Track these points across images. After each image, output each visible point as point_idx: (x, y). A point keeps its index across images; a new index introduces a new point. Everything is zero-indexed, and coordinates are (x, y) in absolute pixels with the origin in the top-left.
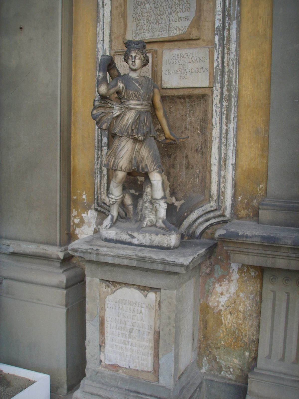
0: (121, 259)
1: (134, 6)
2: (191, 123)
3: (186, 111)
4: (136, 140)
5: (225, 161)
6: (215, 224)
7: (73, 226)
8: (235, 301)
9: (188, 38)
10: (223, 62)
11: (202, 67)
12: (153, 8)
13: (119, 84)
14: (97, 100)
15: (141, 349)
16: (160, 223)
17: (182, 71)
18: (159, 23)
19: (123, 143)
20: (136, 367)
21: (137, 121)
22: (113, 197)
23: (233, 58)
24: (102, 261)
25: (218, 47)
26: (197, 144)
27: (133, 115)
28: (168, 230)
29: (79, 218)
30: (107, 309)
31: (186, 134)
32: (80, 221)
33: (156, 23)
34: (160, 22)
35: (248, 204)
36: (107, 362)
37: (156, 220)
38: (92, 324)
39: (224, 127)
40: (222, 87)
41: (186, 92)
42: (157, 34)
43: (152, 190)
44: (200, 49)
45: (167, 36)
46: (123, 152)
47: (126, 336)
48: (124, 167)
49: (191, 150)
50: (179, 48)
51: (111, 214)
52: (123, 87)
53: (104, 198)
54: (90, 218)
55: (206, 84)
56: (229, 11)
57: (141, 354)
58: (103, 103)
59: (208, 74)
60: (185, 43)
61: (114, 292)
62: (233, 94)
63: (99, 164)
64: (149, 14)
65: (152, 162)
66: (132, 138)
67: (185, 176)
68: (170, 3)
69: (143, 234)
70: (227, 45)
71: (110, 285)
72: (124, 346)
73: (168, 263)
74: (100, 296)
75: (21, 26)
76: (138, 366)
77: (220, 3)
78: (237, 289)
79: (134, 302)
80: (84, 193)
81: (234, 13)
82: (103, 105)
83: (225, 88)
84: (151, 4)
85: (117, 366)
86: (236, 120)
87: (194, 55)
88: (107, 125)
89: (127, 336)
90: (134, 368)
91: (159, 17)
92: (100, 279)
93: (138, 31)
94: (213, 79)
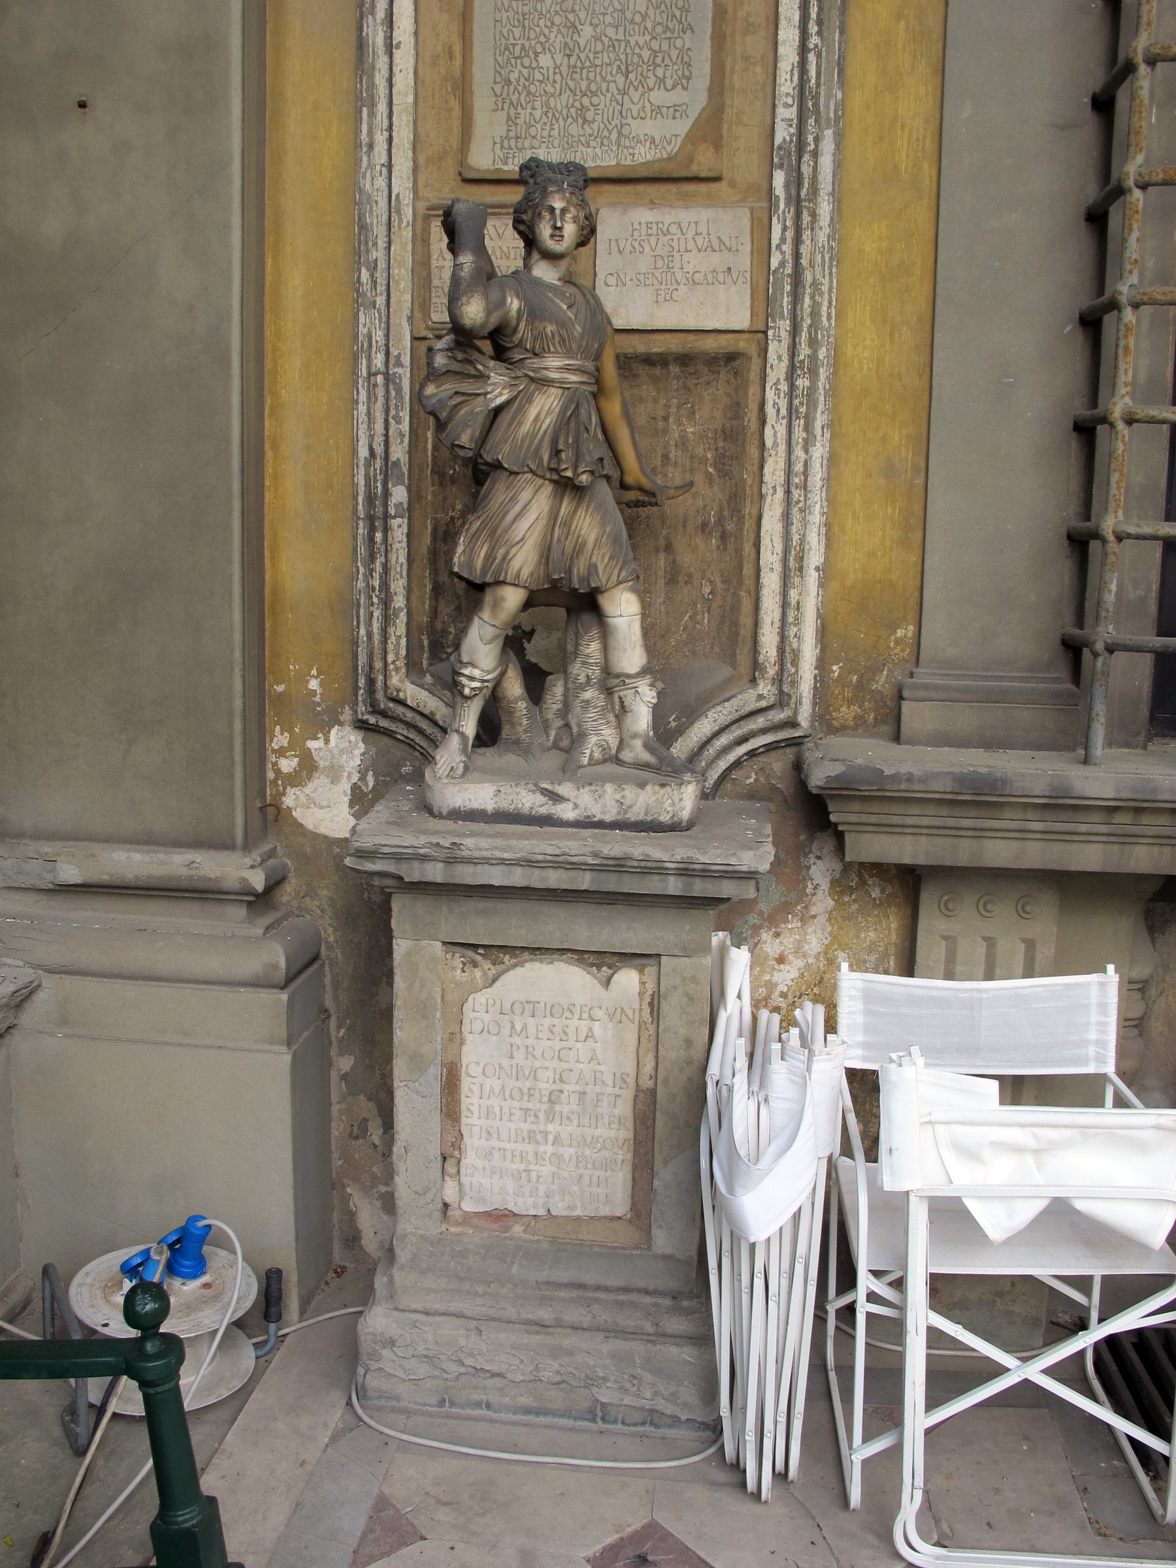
0: (536, 872)
1: (500, 59)
2: (683, 443)
3: (667, 406)
4: (566, 486)
5: (802, 559)
6: (762, 750)
7: (274, 782)
8: (822, 978)
10: (797, 256)
11: (729, 269)
13: (509, 300)
14: (440, 350)
15: (588, 1152)
16: (637, 751)
17: (666, 274)
18: (585, 121)
19: (525, 496)
20: (570, 1208)
21: (569, 419)
22: (477, 673)
23: (823, 246)
24: (469, 881)
25: (782, 206)
26: (705, 507)
27: (556, 403)
30: (469, 1038)
32: (299, 764)
33: (575, 120)
34: (589, 116)
35: (860, 685)
36: (468, 1206)
38: (417, 1092)
39: (799, 452)
40: (795, 332)
41: (674, 344)
43: (605, 648)
44: (721, 210)
45: (613, 163)
46: (524, 525)
47: (536, 1116)
48: (525, 574)
50: (652, 204)
51: (457, 731)
52: (519, 311)
54: (335, 752)
55: (742, 320)
57: (590, 1166)
58: (459, 361)
59: (749, 291)
60: (673, 188)
61: (494, 980)
62: (822, 353)
63: (376, 575)
64: (549, 89)
66: (555, 477)
67: (663, 608)
68: (623, 57)
69: (593, 788)
70: (810, 201)
71: (479, 958)
72: (530, 1148)
73: (706, 873)
74: (443, 997)
75: (84, 98)
76: (578, 1204)
77: (789, 68)
78: (826, 942)
79: (566, 1007)
80: (314, 672)
81: (827, 106)
82: (456, 367)
83: (804, 334)
84: (559, 58)
85: (505, 1216)
86: (827, 435)
87: (702, 228)
89: (542, 1116)
90: (566, 1213)
91: (586, 102)
92: (444, 943)
94: (764, 304)
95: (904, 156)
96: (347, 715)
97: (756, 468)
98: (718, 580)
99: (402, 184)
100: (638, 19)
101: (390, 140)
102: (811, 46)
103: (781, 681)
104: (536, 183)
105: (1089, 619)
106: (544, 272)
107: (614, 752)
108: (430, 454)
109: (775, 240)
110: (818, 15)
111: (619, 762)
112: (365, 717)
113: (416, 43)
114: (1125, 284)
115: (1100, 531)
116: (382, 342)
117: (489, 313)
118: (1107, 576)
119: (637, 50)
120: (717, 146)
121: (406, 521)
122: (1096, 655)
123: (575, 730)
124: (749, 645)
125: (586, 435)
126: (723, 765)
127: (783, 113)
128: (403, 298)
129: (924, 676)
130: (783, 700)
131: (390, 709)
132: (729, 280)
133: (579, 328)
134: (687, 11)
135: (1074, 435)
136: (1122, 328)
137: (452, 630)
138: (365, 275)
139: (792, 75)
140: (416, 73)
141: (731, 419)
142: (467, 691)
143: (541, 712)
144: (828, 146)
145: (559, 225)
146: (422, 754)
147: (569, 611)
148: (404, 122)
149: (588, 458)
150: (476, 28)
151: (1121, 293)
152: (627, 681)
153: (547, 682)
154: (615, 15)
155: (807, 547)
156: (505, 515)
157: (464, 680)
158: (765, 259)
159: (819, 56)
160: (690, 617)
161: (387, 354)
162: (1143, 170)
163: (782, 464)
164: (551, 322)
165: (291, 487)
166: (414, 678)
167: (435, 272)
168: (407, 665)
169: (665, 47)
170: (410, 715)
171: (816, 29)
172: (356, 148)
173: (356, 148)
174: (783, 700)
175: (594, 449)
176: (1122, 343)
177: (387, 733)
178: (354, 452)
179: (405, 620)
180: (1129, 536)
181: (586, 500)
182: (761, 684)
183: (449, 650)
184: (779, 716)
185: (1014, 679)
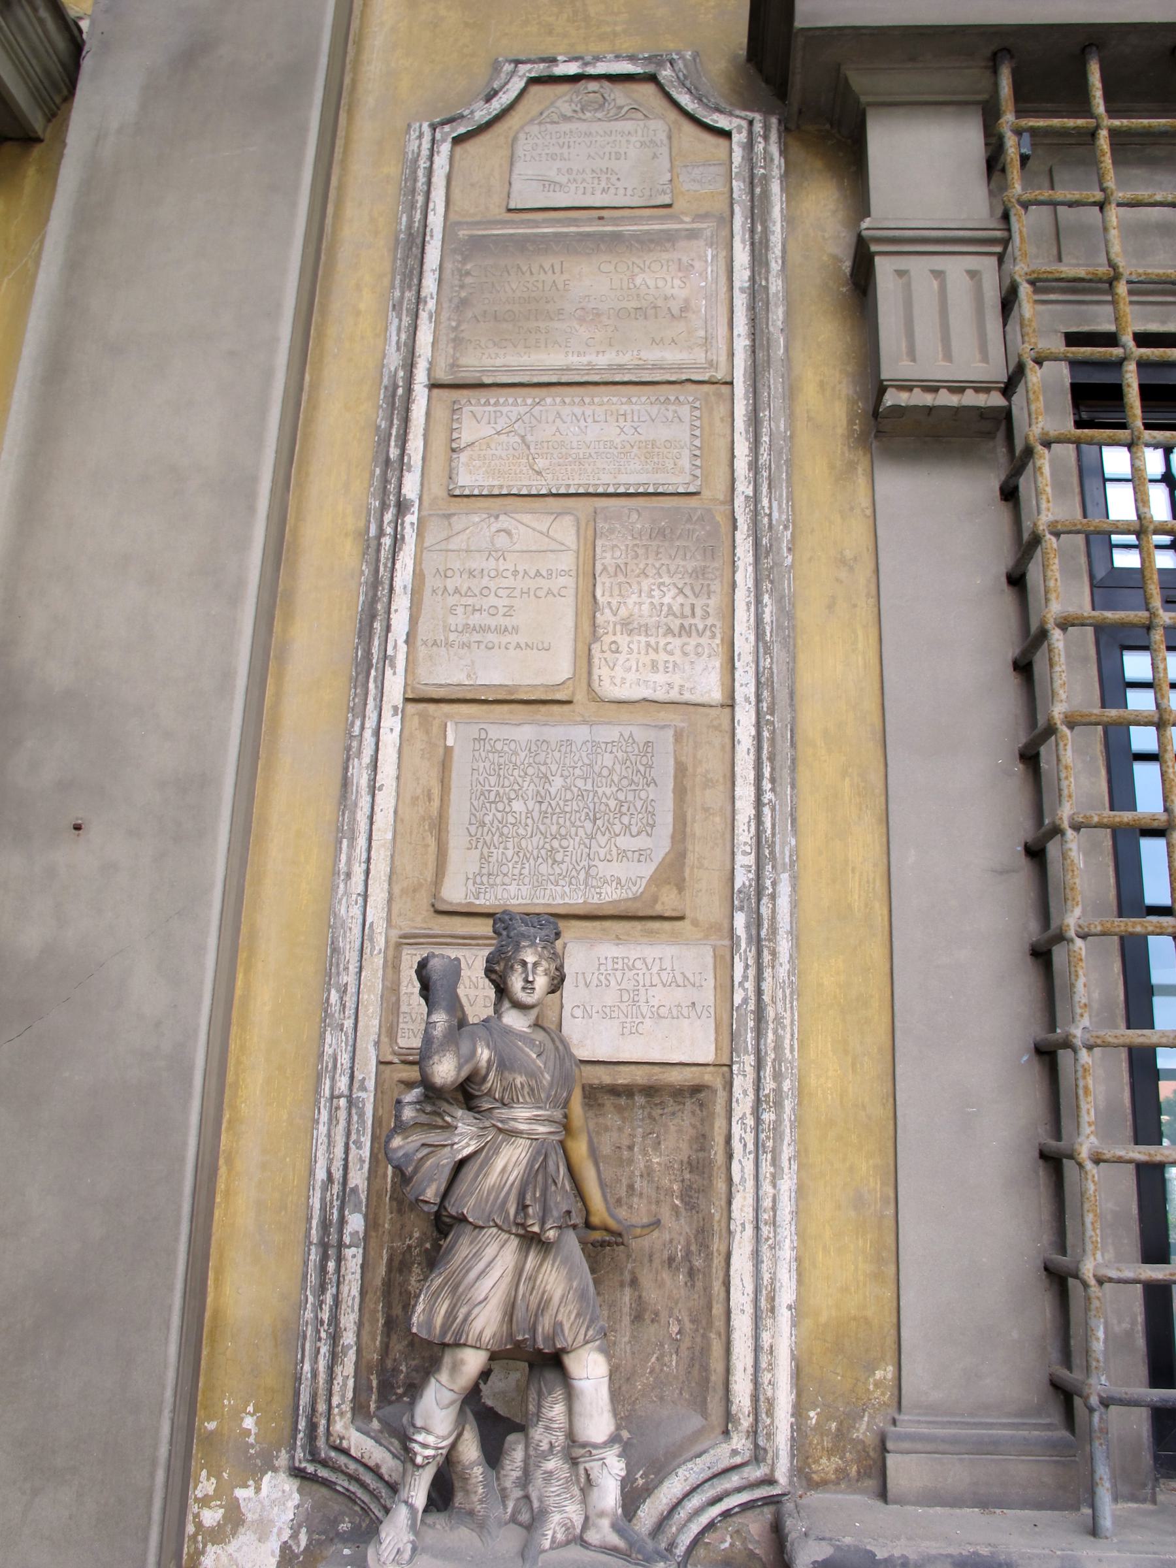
1: (475, 803)
2: (648, 1173)
3: (632, 1136)
4: (531, 1241)
5: (773, 1299)
6: (737, 1510)
9: (650, 913)
10: (759, 992)
12: (536, 815)
13: (479, 1050)
14: (409, 1103)
17: (631, 1008)
18: (555, 861)
19: (490, 1252)
22: (430, 1440)
26: (671, 1241)
27: (523, 1154)
28: (640, 1557)
29: (221, 1506)
31: (631, 1207)
32: (224, 1517)
33: (545, 861)
35: (840, 1435)
37: (582, 1520)
39: (767, 1187)
40: (759, 1066)
41: (639, 1076)
42: (548, 892)
46: (487, 1283)
48: (487, 1335)
49: (651, 1261)
51: (406, 1502)
52: (489, 1061)
53: (343, 1432)
54: (266, 1503)
55: (705, 1052)
56: (772, 845)
59: (713, 1025)
60: (638, 925)
62: (786, 1085)
63: (326, 1308)
64: (521, 831)
65: (578, 1315)
67: (628, 1348)
68: (591, 806)
70: (770, 940)
80: (250, 1409)
81: (783, 852)
82: (423, 1119)
84: (530, 804)
86: (795, 1167)
88: (438, 1189)
91: (556, 844)
93: (485, 879)
94: (729, 1038)
95: (856, 897)
96: (283, 1460)
97: (723, 1203)
98: (686, 1320)
99: (376, 913)
100: (605, 772)
101: (367, 872)
102: (766, 801)
103: (756, 1432)
104: (508, 936)
105: (1077, 1360)
106: (513, 1020)
107: (578, 1531)
108: (389, 1180)
109: (738, 977)
110: (771, 774)
111: (584, 1544)
112: (303, 1465)
113: (398, 786)
114: (1077, 1027)
115: (1080, 1274)
116: (347, 1065)
117: (459, 1068)
118: (1093, 1322)
119: (604, 800)
120: (681, 888)
121: (361, 1250)
122: (1091, 1410)
123: (536, 1504)
124: (720, 1392)
125: (553, 1188)
126: (695, 1528)
127: (741, 860)
128: (371, 1022)
129: (909, 1423)
130: (758, 1455)
131: (331, 1458)
132: (693, 1014)
133: (548, 1077)
134: (651, 767)
135: (1041, 1162)
136: (1080, 1069)
137: (403, 1368)
138: (334, 996)
139: (749, 826)
140: (396, 812)
141: (697, 1151)
142: (419, 1460)
143: (498, 1479)
144: (784, 889)
145: (531, 979)
146: (362, 1508)
147: (531, 1366)
148: (382, 856)
149: (555, 1214)
150: (454, 775)
151: (1075, 1037)
152: (594, 1452)
153: (506, 1445)
154: (584, 769)
155: (778, 1285)
156: (468, 1272)
157: (417, 1448)
158: (729, 995)
159: (773, 810)
160: (658, 1359)
161: (352, 1077)
162: (1081, 922)
163: (750, 1201)
164: (520, 1073)
165: (243, 1206)
166: (359, 1423)
167: (403, 998)
168: (353, 1409)
169: (630, 797)
170: (353, 1467)
171: (769, 786)
172: (334, 875)
173: (334, 875)
174: (758, 1455)
175: (562, 1201)
176: (1081, 1083)
177: (325, 1483)
178: (311, 1173)
179: (354, 1358)
180: (1110, 1280)
181: (551, 1257)
182: (735, 1437)
183: (400, 1391)
184: (757, 1473)
185: (1004, 1426)
